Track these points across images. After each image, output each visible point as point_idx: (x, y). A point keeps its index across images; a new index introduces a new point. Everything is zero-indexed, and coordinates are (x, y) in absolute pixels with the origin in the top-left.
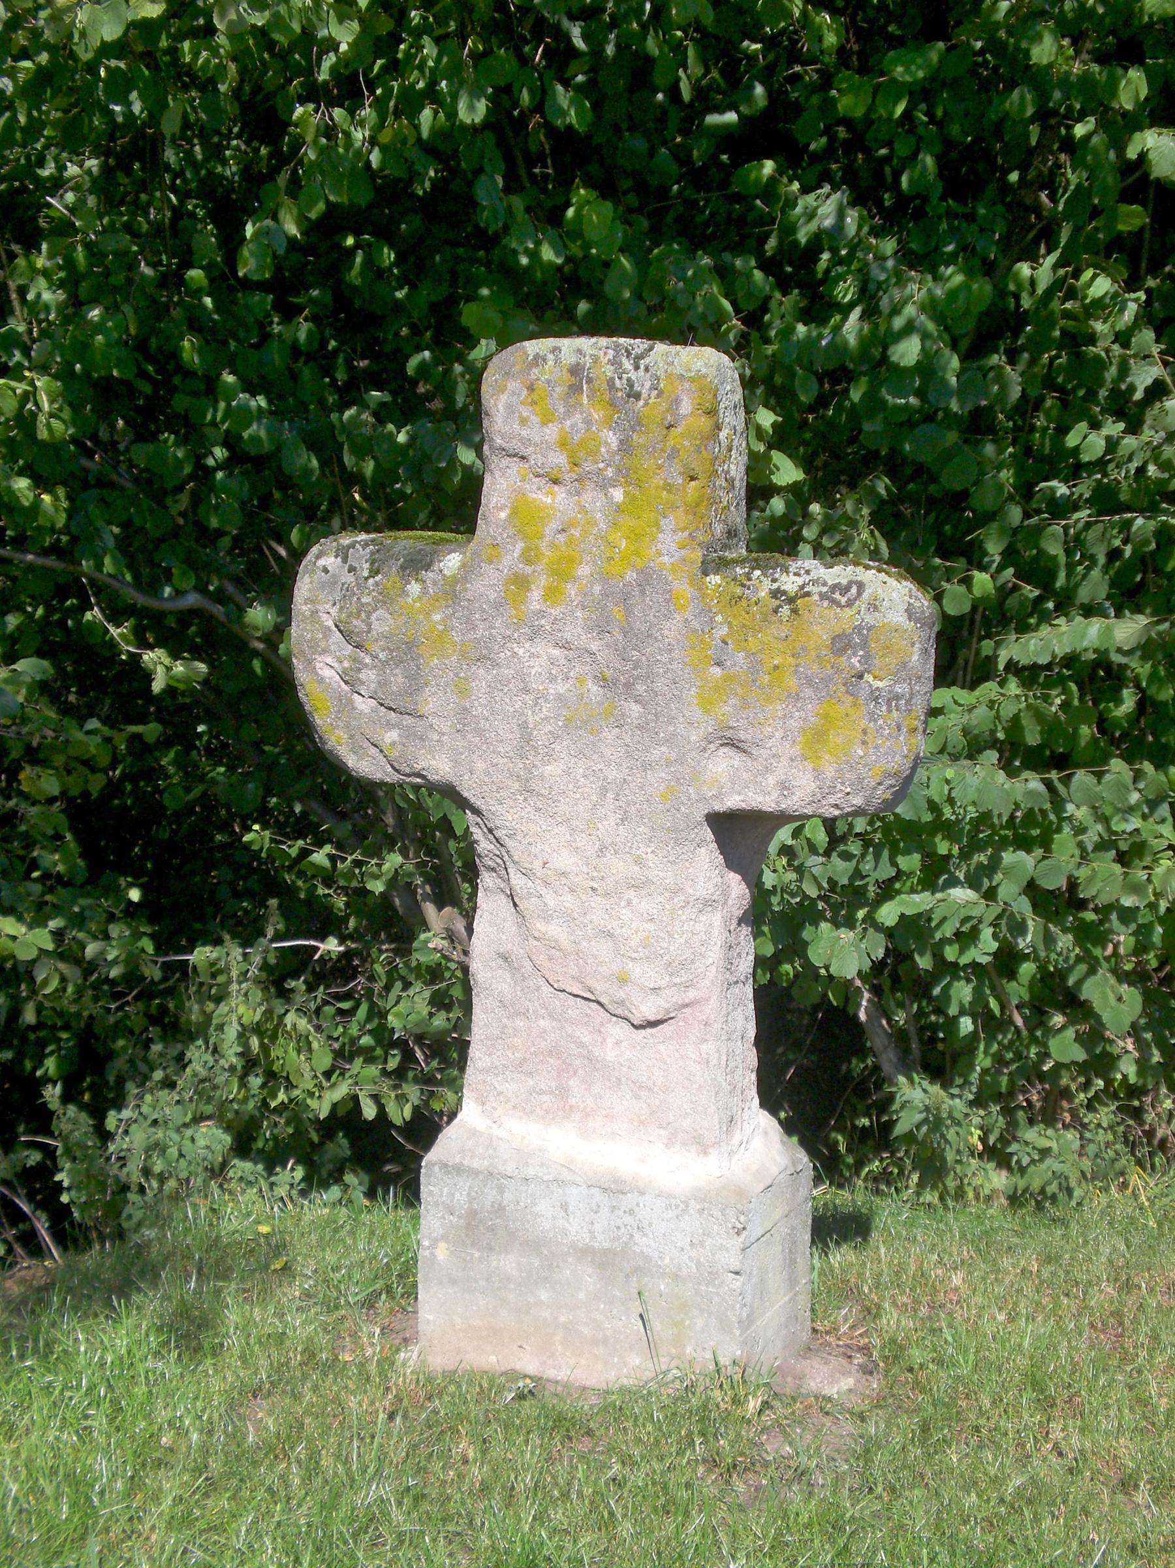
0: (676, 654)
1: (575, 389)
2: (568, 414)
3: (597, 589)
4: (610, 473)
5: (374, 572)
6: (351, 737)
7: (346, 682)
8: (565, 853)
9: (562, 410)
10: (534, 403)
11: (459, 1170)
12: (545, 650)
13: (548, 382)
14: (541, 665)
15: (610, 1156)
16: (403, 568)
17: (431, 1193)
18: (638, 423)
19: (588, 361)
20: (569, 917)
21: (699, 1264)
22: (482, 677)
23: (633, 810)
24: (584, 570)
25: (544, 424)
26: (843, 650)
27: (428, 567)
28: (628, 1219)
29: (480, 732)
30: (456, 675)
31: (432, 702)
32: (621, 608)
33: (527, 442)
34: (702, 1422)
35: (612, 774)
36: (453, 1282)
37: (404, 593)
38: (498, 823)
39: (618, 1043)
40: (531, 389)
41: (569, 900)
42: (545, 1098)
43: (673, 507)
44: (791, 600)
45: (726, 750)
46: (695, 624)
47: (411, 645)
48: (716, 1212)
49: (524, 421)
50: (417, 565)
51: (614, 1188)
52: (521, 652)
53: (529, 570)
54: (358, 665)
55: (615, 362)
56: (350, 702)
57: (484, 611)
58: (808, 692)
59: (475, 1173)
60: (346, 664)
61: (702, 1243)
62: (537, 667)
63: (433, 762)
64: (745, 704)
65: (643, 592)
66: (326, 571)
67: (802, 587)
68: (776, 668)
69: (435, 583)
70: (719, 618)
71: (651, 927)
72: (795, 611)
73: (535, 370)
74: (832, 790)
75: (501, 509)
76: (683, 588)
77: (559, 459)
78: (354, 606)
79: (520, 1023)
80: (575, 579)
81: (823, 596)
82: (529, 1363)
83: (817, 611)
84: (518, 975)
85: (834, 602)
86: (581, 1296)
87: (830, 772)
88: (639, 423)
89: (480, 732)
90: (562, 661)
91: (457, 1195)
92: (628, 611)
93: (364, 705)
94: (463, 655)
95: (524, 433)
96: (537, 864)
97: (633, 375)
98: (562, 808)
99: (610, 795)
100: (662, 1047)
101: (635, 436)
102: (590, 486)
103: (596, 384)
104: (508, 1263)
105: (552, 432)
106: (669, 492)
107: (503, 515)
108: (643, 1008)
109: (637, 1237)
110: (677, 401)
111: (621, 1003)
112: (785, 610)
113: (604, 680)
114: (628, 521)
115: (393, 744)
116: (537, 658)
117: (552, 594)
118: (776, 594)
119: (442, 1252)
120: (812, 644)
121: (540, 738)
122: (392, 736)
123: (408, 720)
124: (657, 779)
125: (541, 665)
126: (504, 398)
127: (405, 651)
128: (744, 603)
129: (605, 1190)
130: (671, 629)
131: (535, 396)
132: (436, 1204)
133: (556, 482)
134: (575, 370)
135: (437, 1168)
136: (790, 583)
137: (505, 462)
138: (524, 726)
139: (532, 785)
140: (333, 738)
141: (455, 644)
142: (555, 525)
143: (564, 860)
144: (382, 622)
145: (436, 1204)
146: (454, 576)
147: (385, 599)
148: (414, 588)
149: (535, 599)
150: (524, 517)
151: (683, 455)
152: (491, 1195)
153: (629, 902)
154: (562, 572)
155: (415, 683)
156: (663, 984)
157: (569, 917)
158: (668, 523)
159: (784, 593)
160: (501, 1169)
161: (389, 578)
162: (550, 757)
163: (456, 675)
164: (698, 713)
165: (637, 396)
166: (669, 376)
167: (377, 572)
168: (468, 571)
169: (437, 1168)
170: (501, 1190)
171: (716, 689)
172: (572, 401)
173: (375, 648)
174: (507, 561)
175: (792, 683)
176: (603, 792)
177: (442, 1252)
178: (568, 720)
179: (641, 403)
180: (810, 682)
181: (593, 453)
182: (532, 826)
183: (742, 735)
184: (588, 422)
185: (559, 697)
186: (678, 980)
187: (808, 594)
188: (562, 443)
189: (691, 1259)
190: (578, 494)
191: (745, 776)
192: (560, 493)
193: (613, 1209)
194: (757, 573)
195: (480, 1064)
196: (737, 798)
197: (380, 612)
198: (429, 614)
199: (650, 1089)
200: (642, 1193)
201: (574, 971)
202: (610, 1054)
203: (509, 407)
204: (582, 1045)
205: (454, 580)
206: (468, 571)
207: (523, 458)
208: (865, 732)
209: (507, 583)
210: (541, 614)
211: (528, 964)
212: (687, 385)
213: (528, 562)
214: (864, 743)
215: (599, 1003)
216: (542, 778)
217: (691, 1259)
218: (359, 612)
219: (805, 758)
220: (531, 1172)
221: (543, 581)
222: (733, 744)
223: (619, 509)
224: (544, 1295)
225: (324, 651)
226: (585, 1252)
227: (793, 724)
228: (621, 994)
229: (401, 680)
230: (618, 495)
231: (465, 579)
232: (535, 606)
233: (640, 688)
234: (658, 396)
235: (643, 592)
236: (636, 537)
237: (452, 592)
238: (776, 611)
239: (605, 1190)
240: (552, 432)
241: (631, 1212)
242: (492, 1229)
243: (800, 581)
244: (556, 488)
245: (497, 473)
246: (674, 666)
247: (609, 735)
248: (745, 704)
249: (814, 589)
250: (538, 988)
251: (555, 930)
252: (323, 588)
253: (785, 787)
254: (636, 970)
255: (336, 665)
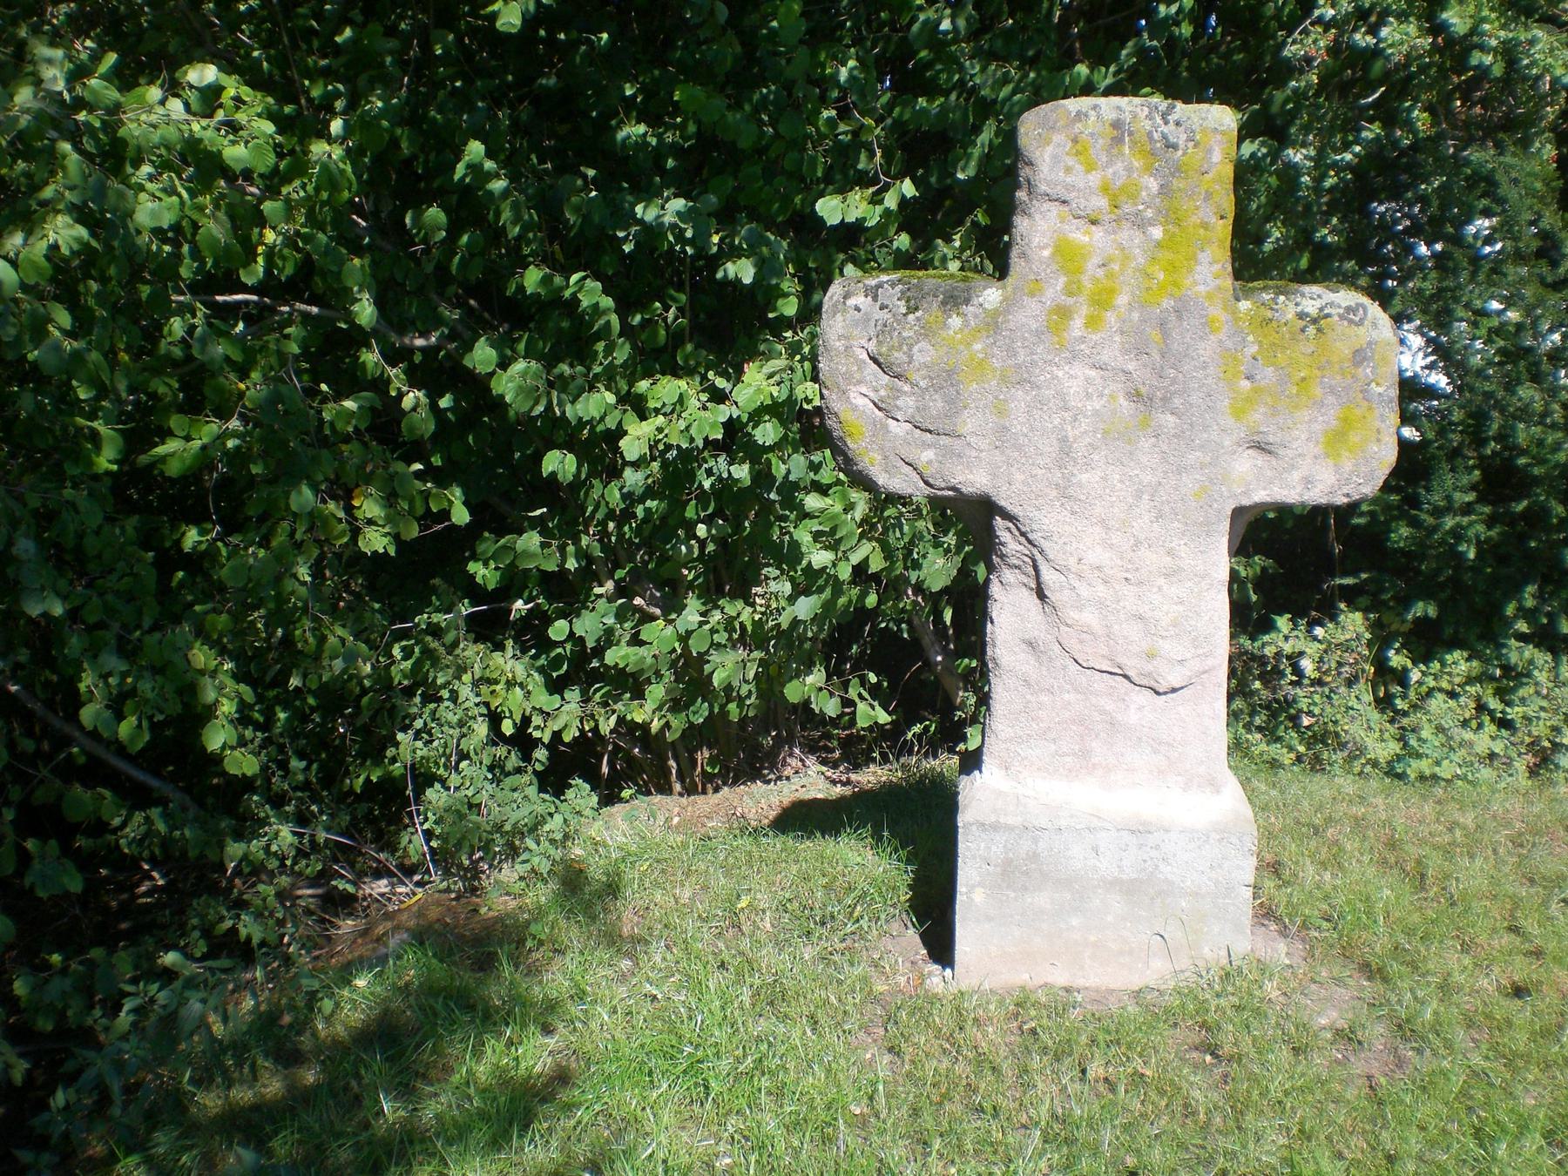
0: (1211, 370)
1: (1118, 141)
2: (1110, 163)
3: (1136, 316)
4: (1149, 213)
5: (912, 310)
6: (886, 458)
7: (880, 409)
8: (1099, 549)
9: (1104, 159)
10: (1078, 153)
11: (995, 827)
12: (1081, 371)
13: (1092, 135)
14: (1081, 384)
15: (1122, 806)
16: (944, 303)
17: (968, 848)
18: (1178, 170)
19: (1128, 117)
20: (1101, 604)
21: (1217, 883)
22: (1020, 399)
23: (1167, 509)
24: (1122, 300)
25: (1088, 172)
26: (1361, 362)
27: (967, 302)
28: (1154, 853)
29: (1019, 448)
30: (996, 398)
31: (969, 423)
32: (1158, 335)
33: (1070, 188)
34: (1209, 1023)
35: (1147, 478)
36: (989, 919)
37: (945, 326)
38: (1035, 527)
39: (1141, 708)
40: (1075, 141)
41: (1101, 590)
42: (1068, 759)
43: (1210, 242)
44: (1315, 321)
45: (1250, 451)
46: (1229, 344)
47: (950, 373)
48: (1234, 840)
49: (1068, 170)
50: (954, 300)
51: (1140, 830)
52: (1060, 374)
53: (1070, 301)
54: (896, 393)
55: (1149, 117)
56: (885, 427)
57: (1025, 339)
58: (1331, 399)
59: (1010, 828)
60: (883, 393)
61: (1220, 866)
62: (1074, 387)
63: (970, 476)
64: (1274, 411)
65: (1180, 318)
66: (858, 309)
67: (1321, 309)
68: (1303, 379)
69: (976, 316)
70: (1251, 338)
71: (1181, 608)
72: (1319, 330)
73: (1079, 125)
74: (1348, 481)
75: (1043, 248)
76: (1217, 312)
77: (1101, 202)
78: (895, 339)
79: (1044, 698)
80: (1114, 308)
81: (1341, 317)
82: (1060, 978)
83: (1339, 330)
84: (1044, 658)
85: (1351, 322)
86: (1110, 918)
87: (1348, 466)
88: (1178, 170)
89: (1019, 448)
90: (1098, 381)
91: (994, 848)
92: (1165, 334)
93: (898, 429)
94: (1004, 379)
95: (1068, 180)
96: (1072, 561)
97: (1165, 129)
98: (1098, 510)
99: (1146, 497)
100: (1180, 708)
101: (1175, 181)
102: (1126, 225)
103: (1137, 136)
104: (1042, 899)
105: (1095, 179)
106: (1206, 229)
107: (1046, 253)
108: (1170, 678)
109: (1162, 867)
110: (1210, 151)
111: (1149, 675)
112: (1311, 330)
113: (1138, 394)
114: (1166, 255)
115: (930, 462)
116: (1074, 379)
117: (1092, 323)
118: (1301, 316)
119: (979, 896)
120: (1335, 359)
121: (1080, 448)
122: (927, 455)
123: (944, 440)
124: (1189, 482)
125: (1081, 384)
126: (1049, 149)
127: (946, 378)
128: (1274, 324)
129: (1133, 832)
130: (1206, 349)
131: (1079, 147)
132: (974, 857)
133: (1094, 222)
134: (1117, 125)
135: (974, 828)
136: (1311, 307)
137: (1047, 205)
138: (1064, 440)
139: (1071, 491)
140: (867, 460)
141: (995, 370)
142: (1096, 260)
143: (1097, 555)
144: (924, 353)
145: (974, 857)
146: (996, 310)
147: (926, 332)
148: (955, 321)
149: (1077, 326)
150: (1068, 258)
151: (1216, 198)
152: (1026, 846)
153: (1160, 588)
154: (1102, 301)
155: (955, 406)
156: (1189, 656)
157: (1101, 604)
158: (1204, 257)
159: (1307, 315)
160: (1036, 824)
161: (931, 311)
162: (1088, 466)
163: (996, 398)
164: (1231, 421)
165: (1175, 147)
166: (1204, 130)
167: (917, 309)
168: (1008, 305)
169: (974, 828)
170: (1035, 840)
171: (1248, 400)
172: (1115, 151)
173: (914, 377)
174: (1049, 293)
175: (1318, 392)
176: (1138, 495)
177: (979, 896)
178: (1105, 432)
179: (1180, 153)
180: (1332, 391)
181: (1134, 197)
182: (1067, 527)
183: (1271, 439)
184: (1129, 169)
185: (1096, 413)
186: (1201, 651)
187: (1328, 316)
188: (1105, 189)
189: (1210, 879)
190: (1115, 232)
191: (1269, 473)
192: (1098, 233)
193: (1140, 846)
194: (1282, 298)
195: (1002, 736)
196: (1263, 493)
197: (923, 344)
198: (969, 344)
199: (1169, 744)
200: (1167, 831)
201: (1105, 651)
202: (1133, 717)
203: (1055, 157)
204: (1103, 712)
205: (996, 313)
206: (1008, 305)
207: (1064, 202)
208: (1378, 431)
209: (1050, 313)
210: (1082, 339)
211: (1057, 647)
212: (1219, 137)
213: (1070, 294)
214: (1378, 440)
215: (1125, 676)
216: (1080, 485)
217: (1210, 879)
218: (900, 346)
219: (1327, 455)
220: (1063, 823)
221: (1084, 310)
222: (1261, 447)
223: (1158, 244)
224: (1075, 922)
225: (859, 382)
226: (1114, 884)
227: (1317, 427)
228: (1150, 668)
229: (940, 404)
230: (1157, 233)
231: (1007, 311)
232: (1077, 333)
233: (1177, 402)
234: (1195, 146)
235: (1180, 318)
236: (1172, 268)
237: (993, 323)
238: (1303, 330)
239: (1133, 832)
240: (1095, 179)
241: (1157, 847)
242: (1026, 873)
243: (1318, 304)
244: (1093, 228)
245: (1037, 217)
246: (1209, 381)
247: (1146, 444)
248: (1274, 411)
249: (1333, 311)
250: (1064, 668)
251: (1089, 617)
252: (857, 325)
253: (1308, 482)
254: (1166, 646)
255: (872, 394)
